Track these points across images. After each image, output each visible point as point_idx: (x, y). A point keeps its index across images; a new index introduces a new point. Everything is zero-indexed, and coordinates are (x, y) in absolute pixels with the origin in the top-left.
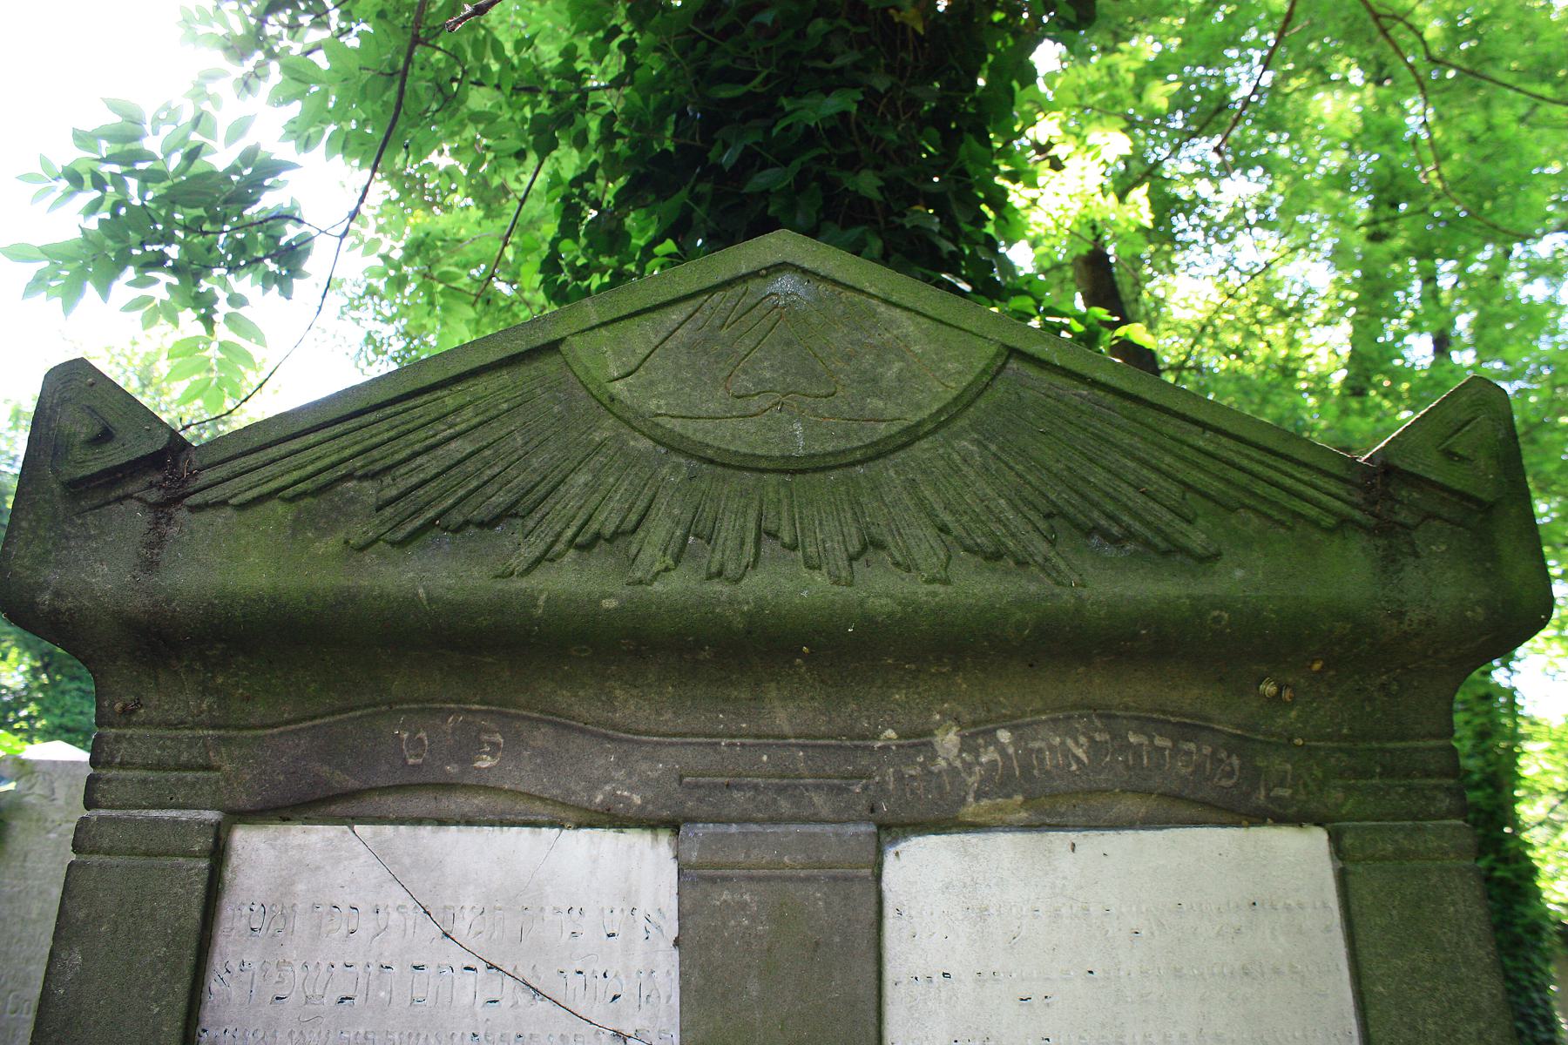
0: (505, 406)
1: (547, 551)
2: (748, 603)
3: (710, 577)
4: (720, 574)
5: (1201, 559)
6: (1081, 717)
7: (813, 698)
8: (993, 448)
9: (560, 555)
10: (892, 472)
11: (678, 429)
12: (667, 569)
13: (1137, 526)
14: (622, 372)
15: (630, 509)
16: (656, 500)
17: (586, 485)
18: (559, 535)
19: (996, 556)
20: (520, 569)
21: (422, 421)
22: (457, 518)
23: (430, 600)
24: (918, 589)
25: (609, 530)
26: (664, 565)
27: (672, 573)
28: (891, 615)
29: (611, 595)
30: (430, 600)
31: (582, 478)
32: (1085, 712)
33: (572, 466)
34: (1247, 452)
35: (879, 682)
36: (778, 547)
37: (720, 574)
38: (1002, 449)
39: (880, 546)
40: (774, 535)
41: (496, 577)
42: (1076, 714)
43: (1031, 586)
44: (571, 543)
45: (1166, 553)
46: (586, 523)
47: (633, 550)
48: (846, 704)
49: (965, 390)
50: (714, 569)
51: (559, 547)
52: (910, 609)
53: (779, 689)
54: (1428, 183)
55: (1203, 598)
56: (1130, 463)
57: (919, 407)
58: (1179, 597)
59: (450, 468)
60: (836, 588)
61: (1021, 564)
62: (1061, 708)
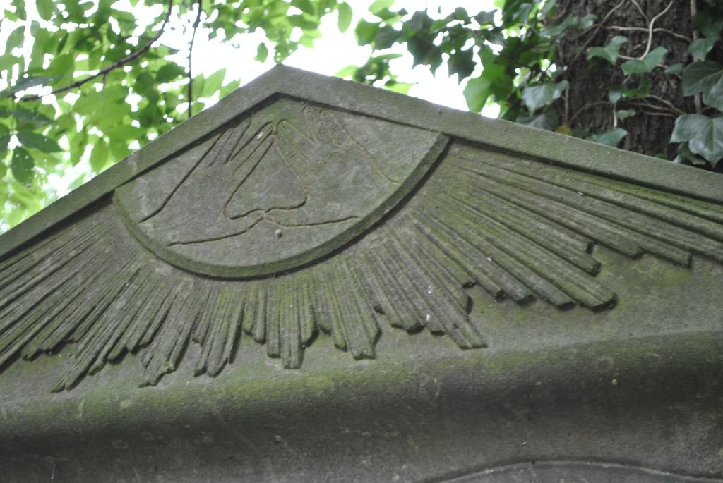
0: (73, 253)
1: (88, 368)
2: (221, 392)
3: (197, 374)
4: (204, 370)
5: (598, 309)
6: (519, 469)
7: (300, 469)
8: (428, 230)
9: (98, 369)
10: (344, 265)
11: (185, 254)
12: (169, 371)
13: (540, 284)
14: (151, 212)
15: (149, 325)
16: (169, 315)
17: (121, 309)
18: (98, 353)
19: (416, 329)
20: (68, 384)
21: (17, 273)
22: (32, 349)
23: (9, 415)
24: (347, 365)
25: (131, 346)
26: (167, 368)
27: (173, 373)
28: (326, 391)
29: (127, 397)
30: (9, 415)
31: (119, 304)
32: (521, 464)
33: (114, 295)
34: (655, 197)
35: (348, 450)
36: (253, 342)
37: (204, 370)
38: (435, 231)
39: (328, 332)
40: (249, 333)
41: (53, 392)
42: (515, 467)
43: (445, 350)
44: (106, 360)
45: (565, 307)
46: (117, 340)
47: (147, 358)
48: (325, 471)
49: (406, 182)
50: (200, 367)
51: (99, 362)
52: (340, 383)
53: (273, 463)
54: (133, 87)
55: (590, 345)
56: (543, 226)
57: (367, 203)
58: (566, 348)
59: (32, 309)
60: (287, 372)
61: (437, 333)
62: (501, 463)
